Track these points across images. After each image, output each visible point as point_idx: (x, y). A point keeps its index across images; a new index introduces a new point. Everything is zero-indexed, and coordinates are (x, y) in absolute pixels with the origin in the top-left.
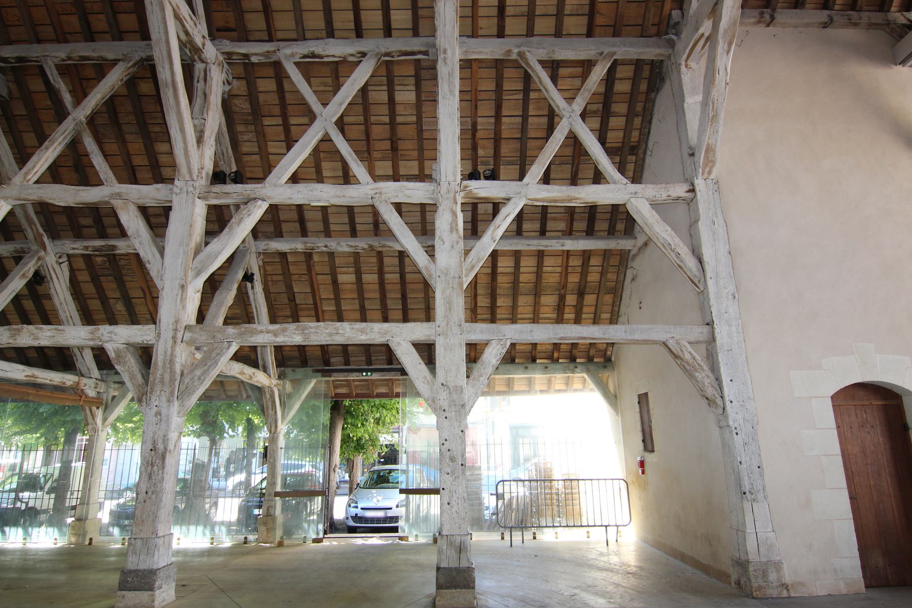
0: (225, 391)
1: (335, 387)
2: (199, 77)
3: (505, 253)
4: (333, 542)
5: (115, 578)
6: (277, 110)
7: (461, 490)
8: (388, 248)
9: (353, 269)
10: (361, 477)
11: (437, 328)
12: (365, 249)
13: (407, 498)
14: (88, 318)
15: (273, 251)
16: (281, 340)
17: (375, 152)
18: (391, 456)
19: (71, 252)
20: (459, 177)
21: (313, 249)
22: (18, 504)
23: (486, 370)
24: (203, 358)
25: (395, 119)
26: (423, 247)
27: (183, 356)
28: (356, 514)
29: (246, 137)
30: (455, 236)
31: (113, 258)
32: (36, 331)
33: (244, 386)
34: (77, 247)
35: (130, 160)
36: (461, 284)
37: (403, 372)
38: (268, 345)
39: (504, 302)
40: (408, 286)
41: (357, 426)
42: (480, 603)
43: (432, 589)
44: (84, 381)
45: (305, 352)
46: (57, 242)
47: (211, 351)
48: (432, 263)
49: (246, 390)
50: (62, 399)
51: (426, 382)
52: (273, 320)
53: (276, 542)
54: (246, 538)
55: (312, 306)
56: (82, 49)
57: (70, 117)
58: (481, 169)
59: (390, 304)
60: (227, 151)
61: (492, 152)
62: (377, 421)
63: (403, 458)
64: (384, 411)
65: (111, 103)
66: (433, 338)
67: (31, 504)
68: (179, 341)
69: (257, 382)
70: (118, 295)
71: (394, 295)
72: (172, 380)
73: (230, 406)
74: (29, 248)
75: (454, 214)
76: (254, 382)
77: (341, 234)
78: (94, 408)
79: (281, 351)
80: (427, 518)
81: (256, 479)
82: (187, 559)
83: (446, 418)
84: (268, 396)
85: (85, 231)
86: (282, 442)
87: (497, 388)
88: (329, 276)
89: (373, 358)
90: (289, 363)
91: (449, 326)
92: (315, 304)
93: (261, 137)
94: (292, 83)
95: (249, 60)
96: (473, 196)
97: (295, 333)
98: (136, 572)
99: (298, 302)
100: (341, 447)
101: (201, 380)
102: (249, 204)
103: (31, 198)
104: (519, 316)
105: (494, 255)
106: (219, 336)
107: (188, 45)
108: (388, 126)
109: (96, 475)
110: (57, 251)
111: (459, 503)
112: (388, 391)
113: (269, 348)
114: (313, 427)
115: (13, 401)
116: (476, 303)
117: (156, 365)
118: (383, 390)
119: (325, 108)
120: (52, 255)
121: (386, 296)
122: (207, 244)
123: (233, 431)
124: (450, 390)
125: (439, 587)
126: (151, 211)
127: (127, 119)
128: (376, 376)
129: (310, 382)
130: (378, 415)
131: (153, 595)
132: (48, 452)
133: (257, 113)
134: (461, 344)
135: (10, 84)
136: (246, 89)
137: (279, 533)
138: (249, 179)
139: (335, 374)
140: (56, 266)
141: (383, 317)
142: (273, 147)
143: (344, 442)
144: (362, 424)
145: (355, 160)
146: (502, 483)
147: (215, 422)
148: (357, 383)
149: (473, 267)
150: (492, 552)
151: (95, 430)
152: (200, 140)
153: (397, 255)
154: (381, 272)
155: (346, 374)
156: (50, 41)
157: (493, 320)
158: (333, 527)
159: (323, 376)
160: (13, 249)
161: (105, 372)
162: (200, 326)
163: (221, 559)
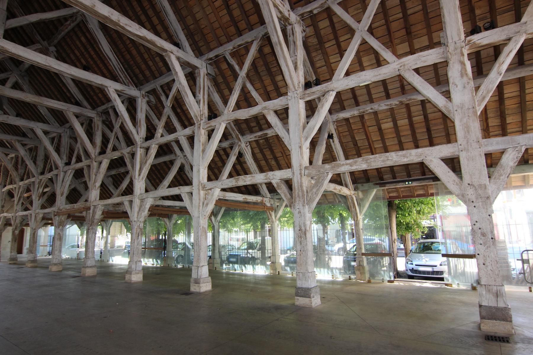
0: (327, 199)
1: (389, 193)
2: (290, 34)
3: (509, 82)
4: (400, 283)
5: (293, 291)
6: (331, 36)
7: (493, 256)
8: (413, 100)
9: (391, 119)
10: (412, 247)
11: (460, 147)
12: (397, 105)
13: (448, 261)
14: (262, 170)
15: (341, 118)
16: (354, 168)
17: (395, 40)
18: (431, 233)
19: (250, 140)
20: (463, 36)
21: (364, 112)
22: (249, 255)
23: (505, 171)
24: (315, 183)
25: (406, 12)
26: (440, 93)
27: (306, 182)
28: (413, 268)
29: (317, 58)
30: (465, 79)
31: (267, 139)
32: (244, 178)
33: (337, 196)
34: (251, 137)
35: (266, 89)
36: (475, 112)
37: (436, 179)
38: (346, 172)
39: (513, 119)
40: (431, 122)
41: (405, 216)
42: (517, 332)
43: (477, 318)
44: (265, 199)
45: (367, 173)
46: (244, 137)
47: (319, 178)
48: (449, 102)
49: (338, 198)
50: (258, 208)
51: (455, 184)
52: (347, 158)
53: (367, 280)
54: (350, 277)
55: (368, 146)
56: (238, 41)
57: (240, 76)
58: (480, 24)
59: (419, 136)
60: (309, 70)
61: (488, 8)
62: (419, 212)
63: (439, 234)
64: (423, 205)
65: (254, 64)
66: (457, 153)
67: (253, 255)
68: (303, 175)
69: (344, 193)
70: (272, 157)
71: (421, 131)
72: (303, 195)
73: (330, 207)
74: (235, 142)
75: (463, 64)
76: (341, 193)
77: (380, 99)
78: (271, 212)
79: (354, 175)
80: (463, 274)
81: (349, 246)
82: (322, 285)
83: (475, 207)
84: (350, 201)
85: (254, 129)
86: (361, 225)
87: (514, 184)
88: (376, 126)
89: (411, 173)
90: (359, 181)
91: (469, 143)
92: (370, 144)
93: (326, 56)
94: (338, 16)
95: (313, 13)
96: (477, 46)
97: (362, 163)
98: (301, 288)
99: (359, 145)
100: (397, 229)
101: (316, 194)
102: (325, 95)
103: (232, 118)
104: (529, 128)
105: (501, 87)
106: (322, 170)
107: (282, 19)
108: (402, 20)
109: (276, 242)
110: (246, 140)
111: (493, 264)
112: (424, 193)
113: (347, 174)
114: (377, 217)
115: (240, 210)
116: (487, 124)
117: (295, 188)
118: (421, 192)
119: (359, 23)
120: (243, 143)
121: (415, 131)
122: (308, 123)
123: (334, 221)
124: (475, 187)
125: (482, 318)
126: (279, 112)
127: (262, 69)
128: (415, 184)
129: (373, 191)
130: (419, 209)
131: (311, 300)
132: (255, 233)
133: (321, 42)
134: (480, 155)
135: (215, 69)
136: (313, 30)
137: (367, 276)
138: (322, 81)
139: (388, 185)
140: (246, 148)
141: (415, 146)
142: (332, 59)
143: (398, 226)
144: (409, 214)
145: (384, 50)
146: (526, 252)
147: (324, 216)
148: (402, 189)
149: (484, 98)
150: (520, 299)
151: (273, 222)
152: (296, 68)
153: (420, 103)
154: (410, 117)
155: (394, 184)
156: (225, 43)
157: (504, 133)
158: (398, 275)
159: (380, 187)
160: (229, 144)
161: (272, 194)
162: (311, 166)
163: (339, 286)
